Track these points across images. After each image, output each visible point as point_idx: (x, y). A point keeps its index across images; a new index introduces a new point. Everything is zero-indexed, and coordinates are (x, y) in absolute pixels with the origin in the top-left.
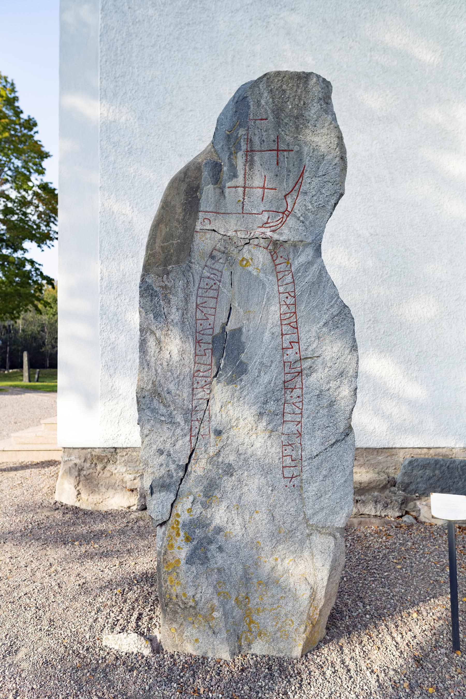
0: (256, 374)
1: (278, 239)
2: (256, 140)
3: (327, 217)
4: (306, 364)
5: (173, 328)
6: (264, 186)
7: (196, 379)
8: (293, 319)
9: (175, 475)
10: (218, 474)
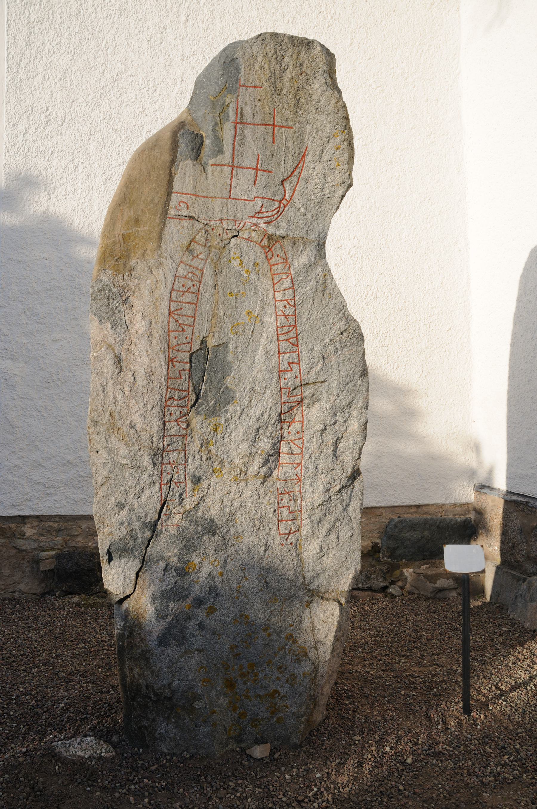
0: (246, 403)
1: (274, 233)
2: (248, 111)
3: (333, 210)
4: (308, 391)
5: (138, 342)
6: (257, 167)
7: (169, 410)
8: (292, 334)
9: (140, 535)
10: (197, 532)
